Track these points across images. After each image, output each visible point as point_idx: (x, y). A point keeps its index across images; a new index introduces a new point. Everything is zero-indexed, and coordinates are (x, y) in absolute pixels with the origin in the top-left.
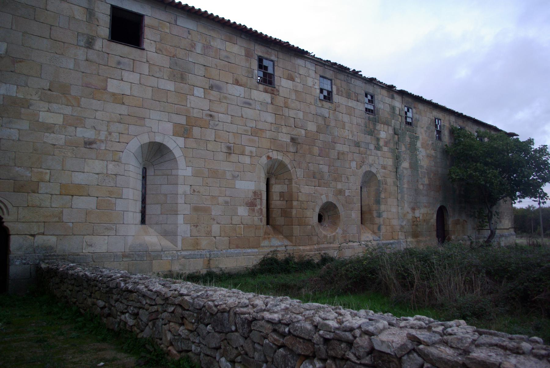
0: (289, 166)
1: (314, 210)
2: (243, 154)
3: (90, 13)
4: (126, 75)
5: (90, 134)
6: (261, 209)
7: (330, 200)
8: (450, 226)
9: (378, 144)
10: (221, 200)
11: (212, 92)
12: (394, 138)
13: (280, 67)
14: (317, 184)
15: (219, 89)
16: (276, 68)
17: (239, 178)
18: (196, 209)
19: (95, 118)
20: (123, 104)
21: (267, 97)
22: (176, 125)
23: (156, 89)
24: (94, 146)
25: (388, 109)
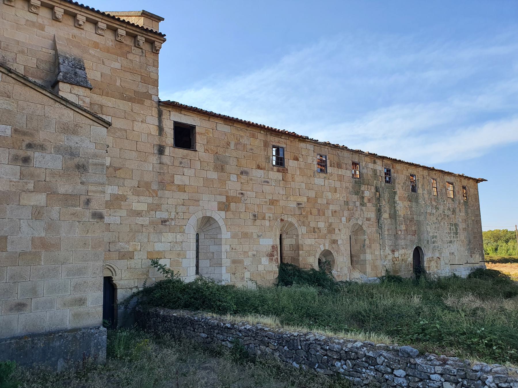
0: (296, 225)
1: (315, 256)
2: (264, 219)
3: (161, 129)
4: (185, 170)
5: (165, 215)
6: (277, 258)
7: (327, 248)
8: (425, 263)
9: (363, 201)
10: (250, 254)
11: (242, 176)
12: (376, 194)
13: (290, 148)
14: (317, 237)
15: (247, 173)
16: (285, 152)
17: (262, 237)
18: (234, 262)
19: (167, 204)
20: (185, 192)
21: (280, 176)
22: (219, 203)
23: (206, 180)
24: (167, 223)
25: (370, 173)
